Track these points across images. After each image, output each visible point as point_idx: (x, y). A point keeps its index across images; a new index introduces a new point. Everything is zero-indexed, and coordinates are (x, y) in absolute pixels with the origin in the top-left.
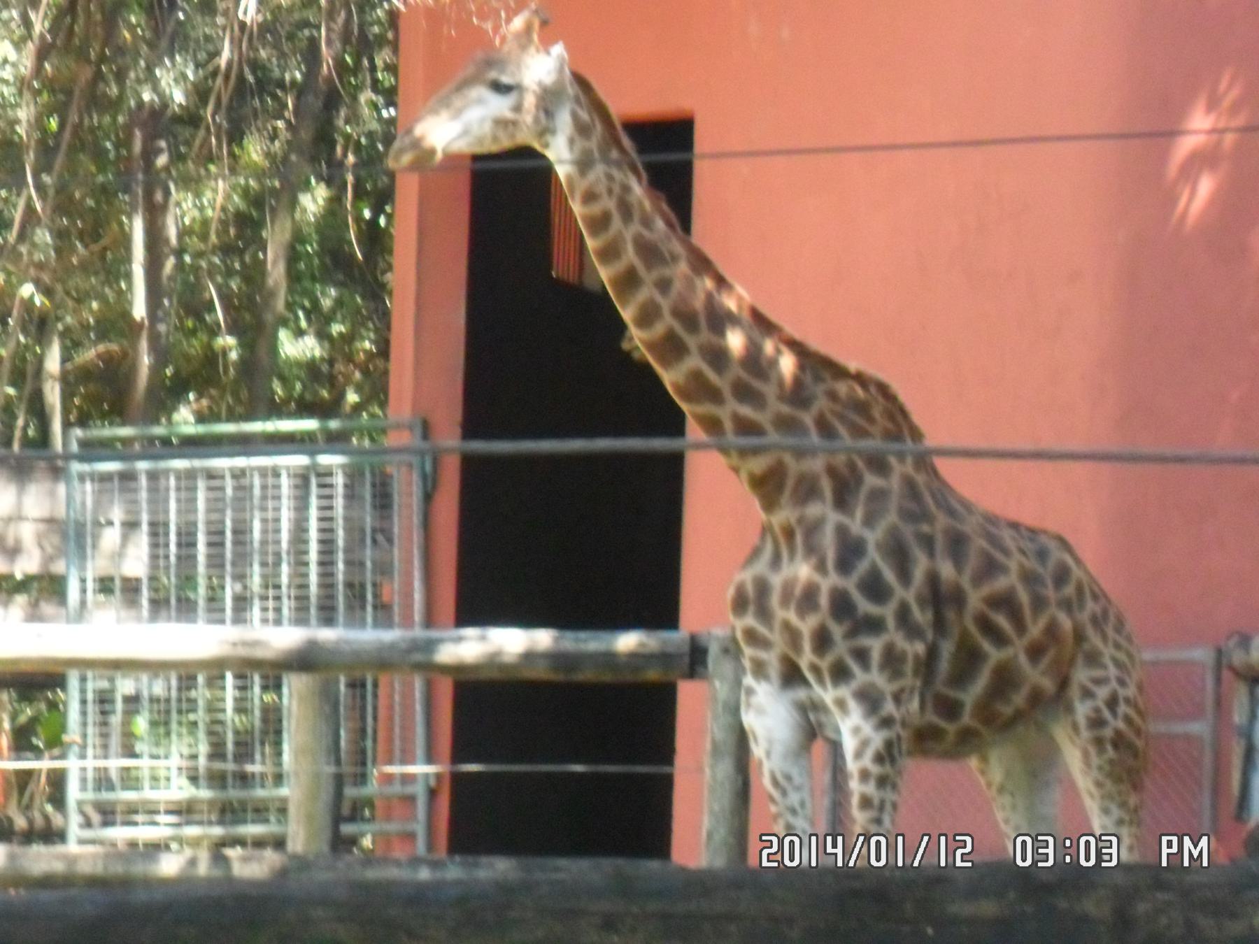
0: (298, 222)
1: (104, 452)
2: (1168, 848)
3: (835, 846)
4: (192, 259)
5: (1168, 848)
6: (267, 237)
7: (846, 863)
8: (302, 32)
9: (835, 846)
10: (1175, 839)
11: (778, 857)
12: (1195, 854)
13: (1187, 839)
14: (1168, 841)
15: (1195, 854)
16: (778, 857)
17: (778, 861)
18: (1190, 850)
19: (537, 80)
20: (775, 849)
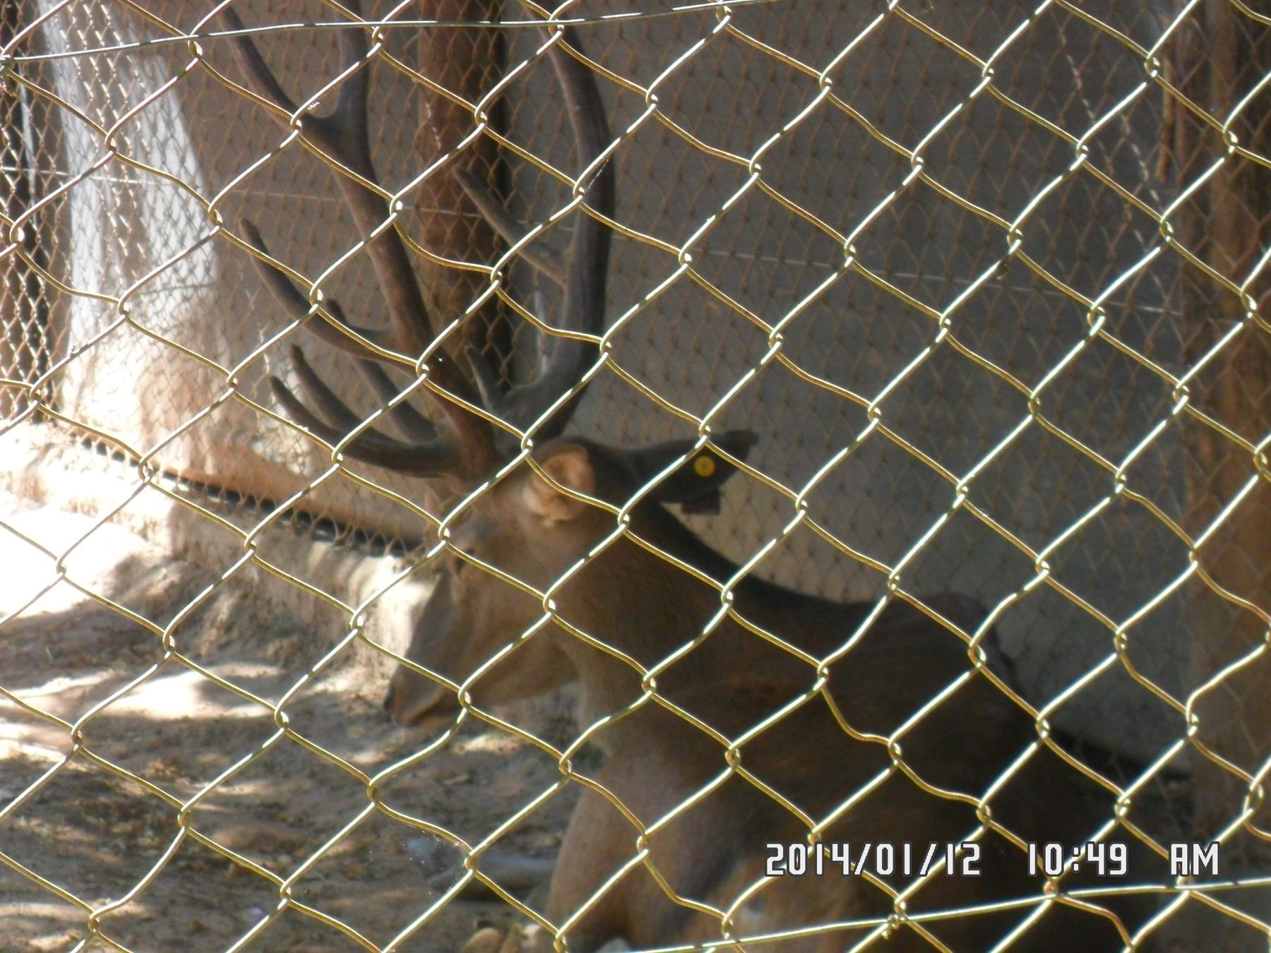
0: (183, 571)
1: (72, 638)
2: (1181, 863)
3: (841, 854)
4: (584, 188)
5: (1181, 863)
6: (195, 212)
7: (852, 872)
8: (302, 472)
9: (841, 854)
10: (1184, 847)
11: (785, 867)
12: (1206, 862)
13: (1196, 847)
14: (1177, 849)
15: (1206, 862)
16: (785, 867)
17: (783, 869)
18: (1200, 860)
19: (45, 508)
20: (780, 857)
